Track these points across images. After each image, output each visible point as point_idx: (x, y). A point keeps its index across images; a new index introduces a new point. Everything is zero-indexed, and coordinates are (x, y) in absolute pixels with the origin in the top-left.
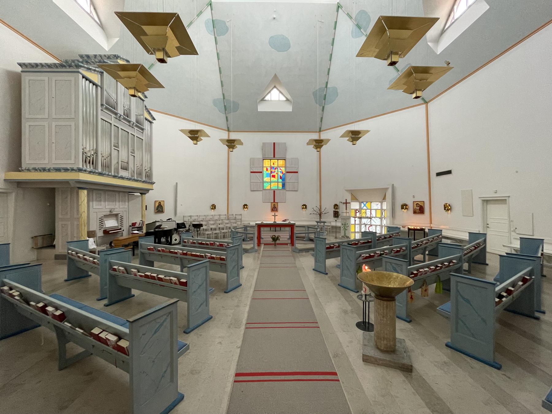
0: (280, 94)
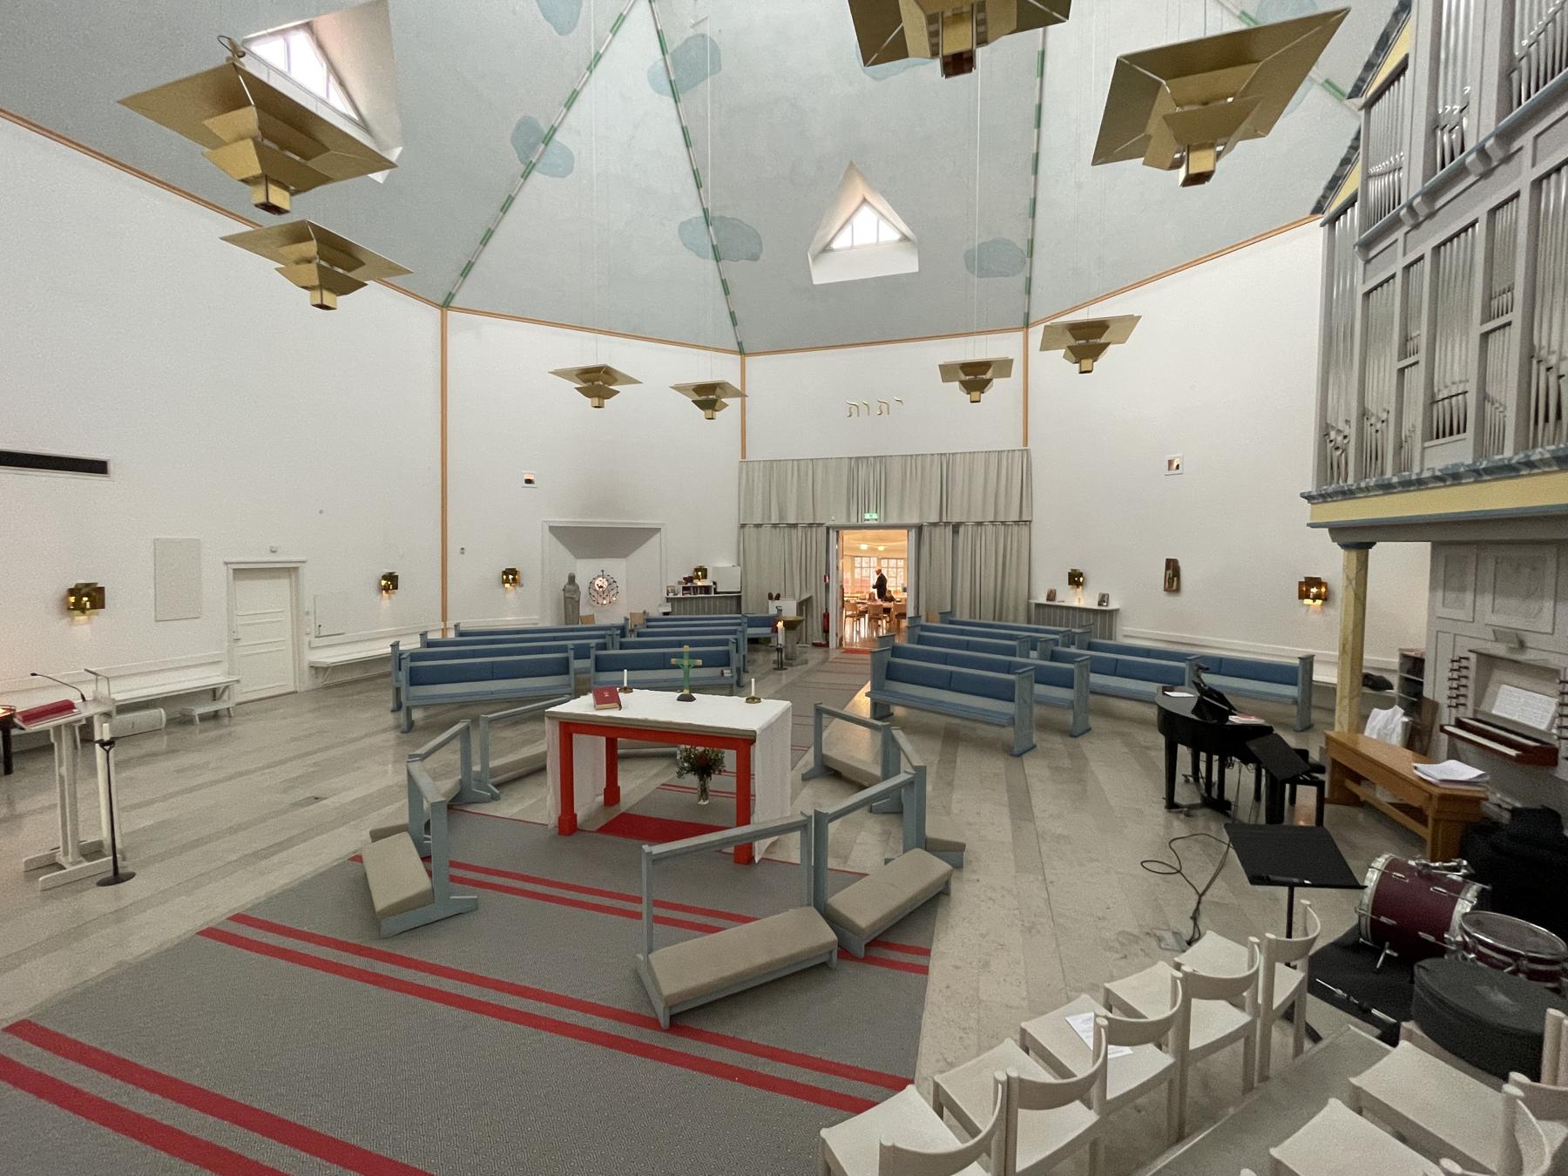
0: (883, 224)
